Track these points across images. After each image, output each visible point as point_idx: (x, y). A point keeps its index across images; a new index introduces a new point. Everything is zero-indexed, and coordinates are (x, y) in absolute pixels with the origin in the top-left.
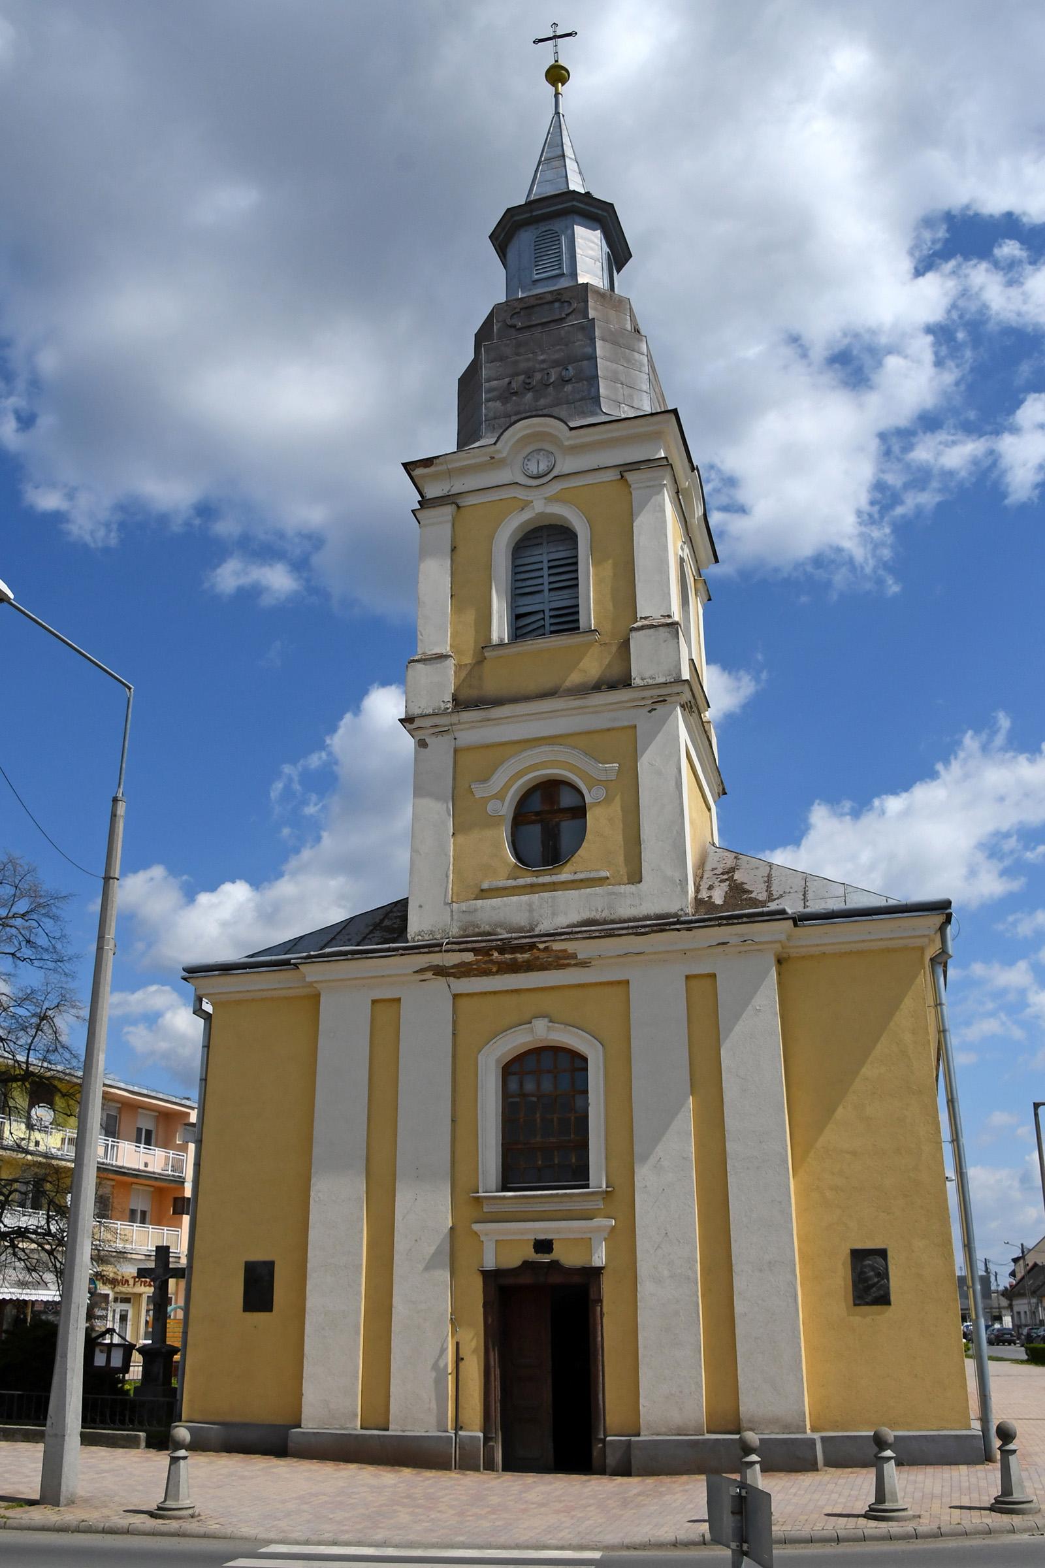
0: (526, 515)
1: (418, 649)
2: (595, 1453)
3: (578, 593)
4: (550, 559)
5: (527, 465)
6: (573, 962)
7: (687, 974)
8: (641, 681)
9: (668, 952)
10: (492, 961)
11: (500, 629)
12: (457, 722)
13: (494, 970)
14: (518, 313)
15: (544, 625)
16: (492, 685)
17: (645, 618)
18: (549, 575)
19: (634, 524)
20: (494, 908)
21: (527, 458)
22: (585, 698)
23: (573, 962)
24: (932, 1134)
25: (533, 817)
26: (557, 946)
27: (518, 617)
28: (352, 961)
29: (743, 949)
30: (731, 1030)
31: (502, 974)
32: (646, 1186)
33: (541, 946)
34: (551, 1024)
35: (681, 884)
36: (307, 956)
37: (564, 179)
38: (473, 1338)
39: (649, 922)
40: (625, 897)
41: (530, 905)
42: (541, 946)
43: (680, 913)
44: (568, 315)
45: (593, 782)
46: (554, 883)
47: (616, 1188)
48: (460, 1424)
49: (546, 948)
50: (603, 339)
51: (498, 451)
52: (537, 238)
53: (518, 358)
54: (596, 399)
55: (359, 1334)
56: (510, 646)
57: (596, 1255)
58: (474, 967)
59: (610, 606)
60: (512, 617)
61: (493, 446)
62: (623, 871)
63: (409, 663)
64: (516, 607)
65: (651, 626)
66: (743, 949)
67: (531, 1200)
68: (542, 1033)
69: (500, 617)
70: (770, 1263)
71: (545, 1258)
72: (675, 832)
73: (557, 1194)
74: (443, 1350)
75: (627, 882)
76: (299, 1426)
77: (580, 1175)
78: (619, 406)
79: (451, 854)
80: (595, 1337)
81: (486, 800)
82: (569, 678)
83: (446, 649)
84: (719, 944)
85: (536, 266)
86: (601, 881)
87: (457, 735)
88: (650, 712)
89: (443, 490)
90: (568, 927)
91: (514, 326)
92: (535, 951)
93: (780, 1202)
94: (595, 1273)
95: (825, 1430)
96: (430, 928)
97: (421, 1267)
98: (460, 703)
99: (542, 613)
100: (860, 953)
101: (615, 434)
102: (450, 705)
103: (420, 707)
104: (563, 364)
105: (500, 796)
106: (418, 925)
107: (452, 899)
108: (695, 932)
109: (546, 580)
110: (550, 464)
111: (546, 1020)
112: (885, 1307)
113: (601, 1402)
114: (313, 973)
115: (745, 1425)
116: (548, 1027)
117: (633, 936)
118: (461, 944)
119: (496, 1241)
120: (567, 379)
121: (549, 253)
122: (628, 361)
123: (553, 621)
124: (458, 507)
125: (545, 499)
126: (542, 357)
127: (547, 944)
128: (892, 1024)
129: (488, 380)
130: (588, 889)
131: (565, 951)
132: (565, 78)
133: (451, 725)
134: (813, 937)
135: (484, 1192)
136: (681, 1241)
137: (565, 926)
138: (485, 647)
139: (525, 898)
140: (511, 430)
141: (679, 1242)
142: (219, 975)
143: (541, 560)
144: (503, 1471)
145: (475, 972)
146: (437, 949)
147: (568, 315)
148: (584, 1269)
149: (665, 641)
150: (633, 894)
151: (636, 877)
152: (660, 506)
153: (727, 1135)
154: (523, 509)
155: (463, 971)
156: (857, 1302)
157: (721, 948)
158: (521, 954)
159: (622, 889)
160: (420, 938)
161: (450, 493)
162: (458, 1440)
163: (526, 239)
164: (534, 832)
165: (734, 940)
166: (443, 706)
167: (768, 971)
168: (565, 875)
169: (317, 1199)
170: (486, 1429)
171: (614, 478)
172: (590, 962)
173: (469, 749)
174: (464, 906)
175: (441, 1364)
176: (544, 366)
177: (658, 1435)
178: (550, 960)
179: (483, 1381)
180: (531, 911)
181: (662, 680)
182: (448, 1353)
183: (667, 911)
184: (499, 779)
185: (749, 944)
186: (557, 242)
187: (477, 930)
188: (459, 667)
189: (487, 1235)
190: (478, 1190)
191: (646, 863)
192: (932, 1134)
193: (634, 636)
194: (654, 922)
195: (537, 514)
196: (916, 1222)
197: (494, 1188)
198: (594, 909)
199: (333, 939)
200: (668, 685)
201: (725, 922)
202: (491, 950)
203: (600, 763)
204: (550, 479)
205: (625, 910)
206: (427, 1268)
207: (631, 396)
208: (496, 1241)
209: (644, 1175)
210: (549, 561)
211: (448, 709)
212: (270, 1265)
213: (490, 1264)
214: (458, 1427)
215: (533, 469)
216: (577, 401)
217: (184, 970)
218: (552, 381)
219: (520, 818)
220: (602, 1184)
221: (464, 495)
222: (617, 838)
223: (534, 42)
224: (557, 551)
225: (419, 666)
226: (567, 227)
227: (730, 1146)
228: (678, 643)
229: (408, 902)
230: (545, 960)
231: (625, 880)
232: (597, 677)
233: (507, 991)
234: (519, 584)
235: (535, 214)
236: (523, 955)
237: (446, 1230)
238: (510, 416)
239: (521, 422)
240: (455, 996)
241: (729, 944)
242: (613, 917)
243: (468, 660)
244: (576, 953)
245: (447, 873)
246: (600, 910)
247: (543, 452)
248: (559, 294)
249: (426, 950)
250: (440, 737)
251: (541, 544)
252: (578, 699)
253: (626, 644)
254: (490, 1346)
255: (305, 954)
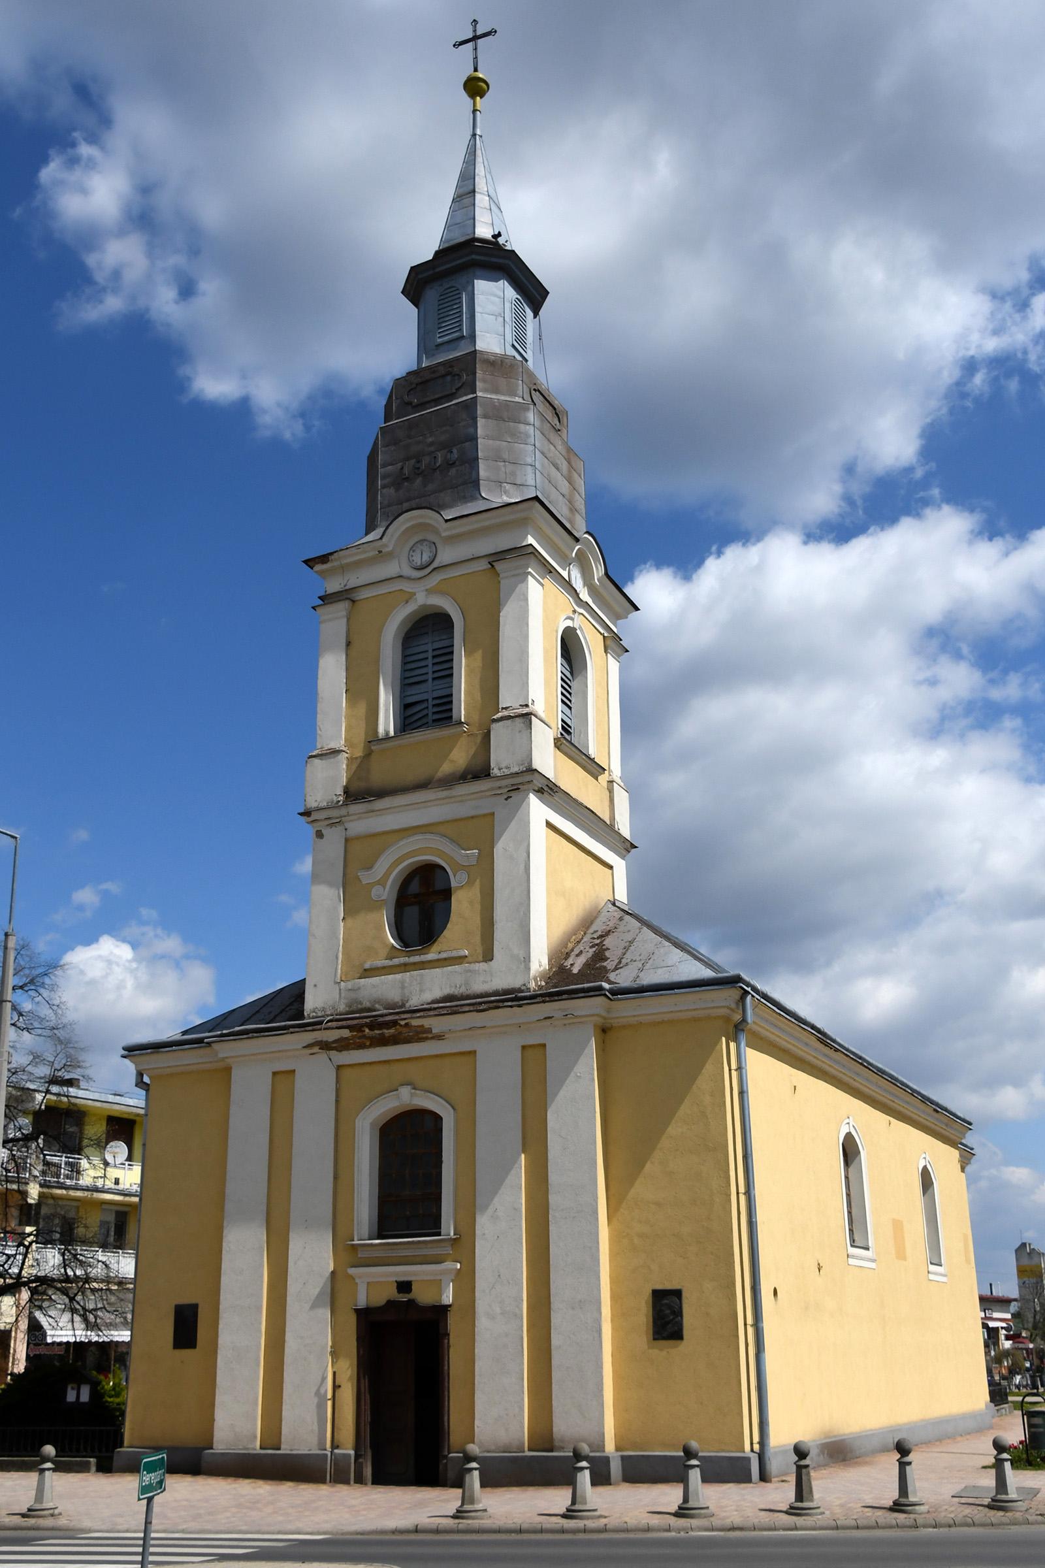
0: (410, 608)
1: (318, 744)
2: (441, 1467)
3: (452, 682)
4: (434, 648)
5: (412, 556)
6: (430, 1036)
7: (547, 1045)
8: (498, 771)
9: (506, 1025)
10: (364, 1037)
11: (387, 722)
12: (346, 814)
13: (368, 1043)
14: (415, 388)
15: (427, 714)
16: (379, 775)
17: (506, 708)
18: (433, 664)
19: (501, 614)
20: (374, 986)
21: (412, 549)
22: (451, 789)
23: (430, 1036)
24: (723, 1187)
25: (412, 899)
26: (415, 1022)
27: (407, 706)
28: (252, 1040)
29: (566, 1022)
30: (556, 1095)
31: (374, 1047)
32: (484, 1234)
33: (403, 1023)
34: (413, 1091)
35: (524, 961)
36: (220, 1034)
37: (472, 221)
38: (348, 1368)
39: (493, 998)
40: (479, 974)
41: (402, 982)
42: (403, 1023)
43: (523, 988)
44: (457, 389)
45: (459, 867)
46: (423, 962)
47: (462, 1237)
48: (335, 1444)
49: (407, 1024)
50: (485, 417)
51: (386, 546)
52: (441, 295)
53: (410, 441)
54: (476, 483)
55: (258, 1365)
56: (394, 739)
57: (445, 1295)
58: (351, 1041)
59: (478, 696)
60: (400, 705)
61: (380, 541)
62: (480, 950)
63: (309, 758)
64: (404, 697)
65: (509, 718)
66: (566, 1022)
67: (399, 1247)
68: (406, 1099)
69: (387, 711)
70: (581, 1301)
71: (404, 1298)
72: (522, 913)
73: (413, 1241)
74: (324, 1379)
75: (482, 960)
76: (212, 1448)
77: (433, 1225)
78: (501, 486)
79: (342, 936)
80: (443, 1366)
81: (372, 885)
82: (441, 769)
83: (340, 743)
84: (545, 1018)
85: (439, 328)
86: (460, 960)
87: (347, 825)
88: (506, 799)
89: (340, 584)
90: (433, 1002)
91: (410, 403)
92: (398, 1027)
93: (590, 1248)
94: (444, 1310)
95: (627, 1450)
96: (322, 1005)
97: (307, 1306)
98: (353, 795)
99: (426, 702)
100: (671, 1022)
101: (487, 523)
102: (341, 798)
103: (316, 801)
104: (447, 446)
105: (382, 882)
106: (314, 1002)
107: (341, 978)
108: (525, 1008)
109: (430, 669)
110: (431, 555)
111: (409, 1087)
112: (679, 1342)
113: (446, 1424)
114: (227, 1050)
115: (557, 1444)
116: (411, 1093)
117: (475, 1013)
118: (339, 1021)
119: (368, 1283)
120: (451, 462)
121: (451, 313)
122: (513, 435)
123: (436, 710)
124: (354, 601)
125: (427, 590)
126: (430, 440)
127: (406, 1021)
128: (694, 1086)
129: (384, 466)
130: (450, 967)
131: (422, 1026)
132: (485, 91)
133: (341, 817)
134: (627, 1010)
135: (358, 1240)
136: (511, 1282)
137: (429, 1000)
138: (373, 740)
139: (398, 976)
140: (401, 518)
141: (509, 1283)
142: (151, 1053)
143: (426, 649)
144: (373, 1484)
145: (353, 1046)
146: (319, 1027)
147: (457, 389)
148: (435, 1306)
149: (520, 731)
150: (485, 971)
151: (488, 956)
152: (524, 594)
153: (550, 1188)
154: (407, 602)
155: (342, 1045)
156: (656, 1337)
157: (548, 1022)
158: (388, 1029)
159: (477, 966)
160: (314, 1014)
161: (347, 588)
162: (333, 1457)
163: (431, 295)
164: (412, 913)
165: (558, 1014)
166: (335, 798)
167: (589, 1040)
168: (431, 956)
169: (228, 1249)
170: (357, 1448)
171: (485, 567)
172: (444, 1036)
173: (358, 838)
174: (350, 985)
175: (322, 1391)
176: (432, 449)
177: (488, 1452)
178: (411, 1034)
179: (355, 1407)
180: (403, 988)
181: (515, 769)
182: (327, 1383)
183: (512, 987)
184: (382, 866)
185: (571, 1018)
186: (457, 301)
187: (360, 1006)
188: (350, 760)
189: (360, 1277)
190: (354, 1238)
191: (497, 943)
192: (723, 1187)
193: (495, 727)
194: (498, 998)
195: (420, 606)
196: (706, 1266)
197: (367, 1236)
198: (453, 985)
199: (248, 1020)
200: (519, 775)
201: (547, 999)
202: (363, 1027)
203: (463, 849)
204: (429, 572)
205: (480, 985)
206: (313, 1307)
207: (513, 474)
208: (368, 1283)
209: (484, 1224)
210: (434, 650)
211: (339, 801)
212: (194, 1308)
213: (362, 1303)
214: (335, 1446)
215: (417, 560)
216: (459, 486)
217: (124, 1049)
218: (438, 465)
219: (403, 900)
220: (450, 1233)
221: (357, 589)
222: (476, 921)
223: (454, 45)
224: (440, 640)
225: (316, 761)
226: (468, 282)
227: (553, 1199)
228: (531, 733)
229: (305, 984)
230: (406, 1034)
231: (481, 958)
232: (464, 767)
233: (380, 1062)
234: (408, 674)
235: (438, 270)
236: (389, 1031)
237: (327, 1274)
238: (401, 504)
239: (403, 515)
240: (339, 1068)
241: (553, 1018)
242: (469, 992)
243: (359, 753)
244: (431, 1028)
245: (337, 955)
246: (458, 986)
247: (426, 543)
248: (451, 367)
249: (310, 1028)
250: (333, 828)
251: (427, 633)
252: (446, 790)
253: (487, 736)
254: (362, 1376)
255: (219, 1033)
